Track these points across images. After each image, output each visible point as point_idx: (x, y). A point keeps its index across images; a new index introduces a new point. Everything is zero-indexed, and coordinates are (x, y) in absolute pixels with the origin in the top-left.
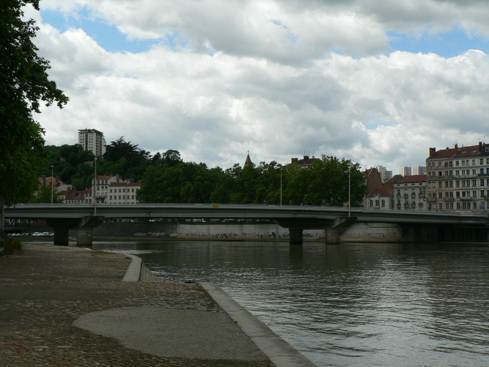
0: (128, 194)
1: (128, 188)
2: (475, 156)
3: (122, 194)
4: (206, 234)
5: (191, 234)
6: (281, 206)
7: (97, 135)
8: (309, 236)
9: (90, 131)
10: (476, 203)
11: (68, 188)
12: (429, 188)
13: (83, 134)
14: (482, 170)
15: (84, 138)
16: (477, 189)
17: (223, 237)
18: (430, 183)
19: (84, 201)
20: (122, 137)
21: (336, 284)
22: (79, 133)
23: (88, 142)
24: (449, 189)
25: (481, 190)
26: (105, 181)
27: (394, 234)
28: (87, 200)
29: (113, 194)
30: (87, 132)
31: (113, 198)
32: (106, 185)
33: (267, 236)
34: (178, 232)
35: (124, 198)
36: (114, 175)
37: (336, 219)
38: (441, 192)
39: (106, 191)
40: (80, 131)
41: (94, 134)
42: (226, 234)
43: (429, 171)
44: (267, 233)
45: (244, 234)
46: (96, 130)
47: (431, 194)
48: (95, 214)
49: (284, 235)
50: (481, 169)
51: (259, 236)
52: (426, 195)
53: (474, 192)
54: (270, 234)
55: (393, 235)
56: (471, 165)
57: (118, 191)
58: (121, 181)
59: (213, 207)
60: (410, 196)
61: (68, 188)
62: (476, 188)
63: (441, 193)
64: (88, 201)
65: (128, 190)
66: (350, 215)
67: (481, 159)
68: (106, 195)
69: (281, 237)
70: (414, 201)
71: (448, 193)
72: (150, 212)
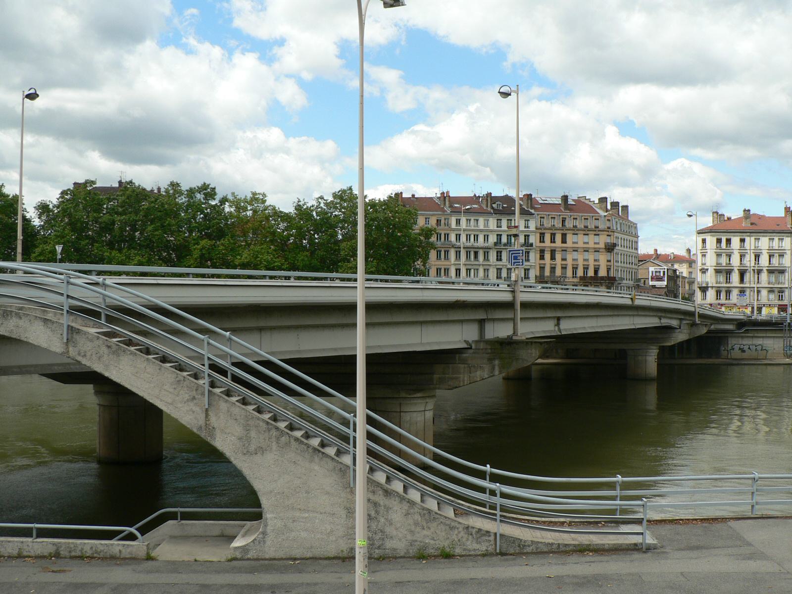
14: (499, 236)
24: (442, 263)
25: (498, 267)
50: (497, 235)
53: (486, 271)
67: (498, 220)
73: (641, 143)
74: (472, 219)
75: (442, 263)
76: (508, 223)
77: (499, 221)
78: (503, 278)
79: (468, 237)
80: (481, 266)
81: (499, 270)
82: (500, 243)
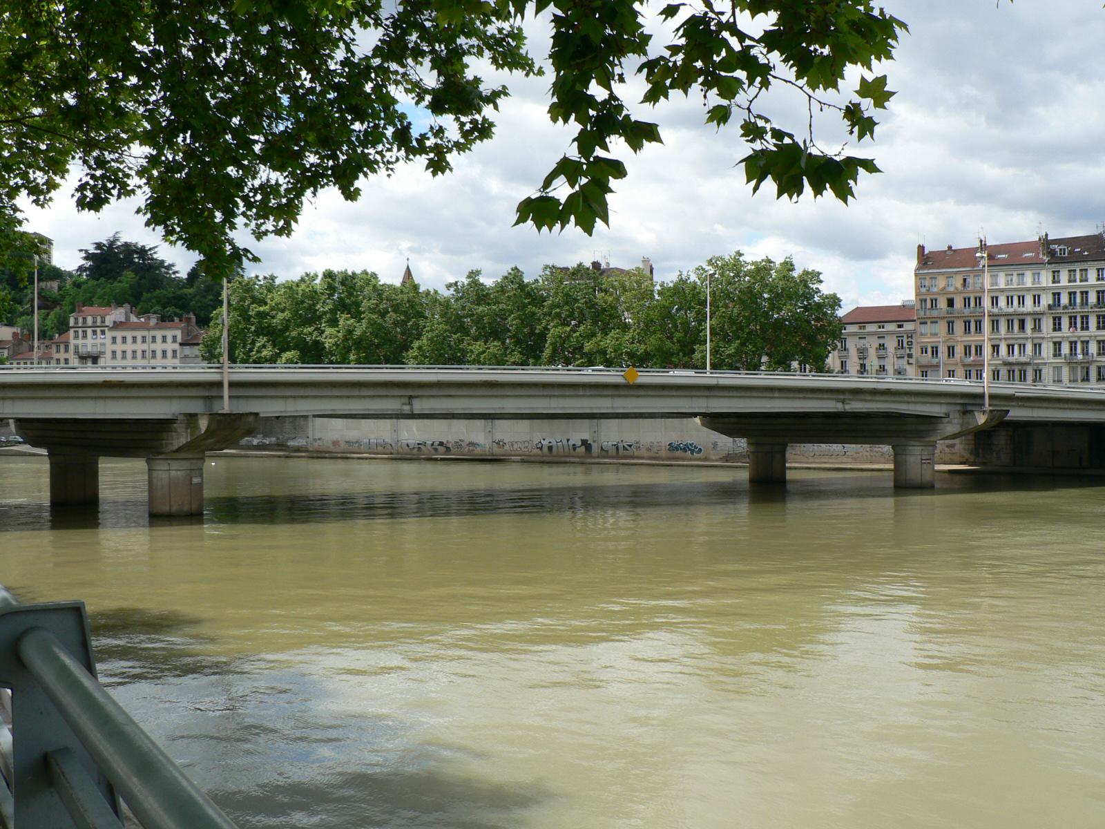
0: (153, 346)
1: (153, 333)
2: (1034, 264)
3: (140, 347)
4: (388, 440)
6: (708, 374)
8: (690, 450)
10: (1040, 371)
11: (14, 333)
12: (922, 334)
14: (1057, 296)
16: (1043, 338)
17: (436, 450)
18: (926, 323)
20: (117, 233)
24: (973, 338)
25: (1055, 340)
26: (99, 319)
27: (947, 447)
31: (119, 355)
32: (102, 329)
33: (566, 449)
34: (310, 434)
35: (143, 357)
38: (951, 344)
39: (103, 341)
42: (445, 442)
43: (924, 297)
44: (565, 442)
45: (499, 443)
47: (926, 349)
48: (226, 406)
49: (617, 448)
50: (1054, 294)
51: (541, 449)
52: (913, 351)
53: (1037, 347)
54: (574, 445)
55: (946, 449)
56: (1002, 285)
57: (129, 340)
58: (133, 319)
59: (620, 380)
61: (14, 333)
62: (1042, 336)
63: (953, 347)
65: (154, 338)
66: (990, 405)
67: (1054, 272)
68: (103, 350)
69: (607, 451)
70: (882, 364)
71: (970, 347)
72: (411, 397)
73: (779, 130)
74: (1078, 270)
75: (973, 338)
76: (1070, 275)
77: (1084, 273)
78: (1063, 356)
79: (1009, 300)
80: (1003, 341)
81: (1058, 345)
82: (1059, 305)
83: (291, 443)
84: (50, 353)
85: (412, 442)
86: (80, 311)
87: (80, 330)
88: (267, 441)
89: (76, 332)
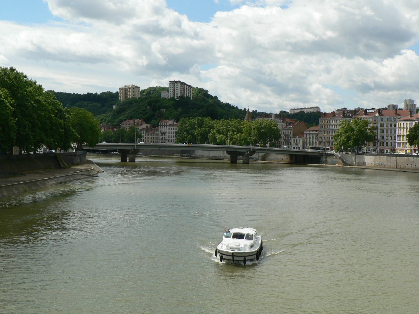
5: (201, 156)
7: (181, 85)
9: (177, 82)
13: (172, 84)
15: (173, 87)
19: (155, 134)
21: (54, 175)
22: (169, 83)
23: (175, 90)
24: (328, 135)
26: (166, 123)
28: (156, 134)
29: (170, 131)
30: (174, 82)
32: (166, 126)
34: (195, 154)
36: (172, 120)
37: (246, 152)
39: (166, 129)
40: (170, 82)
41: (180, 84)
46: (181, 81)
48: (136, 148)
58: (175, 123)
60: (311, 137)
64: (157, 134)
71: (383, 133)
72: (160, 147)
83: (192, 156)
84: (154, 132)
85: (212, 156)
86: (162, 121)
87: (161, 126)
88: (188, 155)
89: (160, 127)
